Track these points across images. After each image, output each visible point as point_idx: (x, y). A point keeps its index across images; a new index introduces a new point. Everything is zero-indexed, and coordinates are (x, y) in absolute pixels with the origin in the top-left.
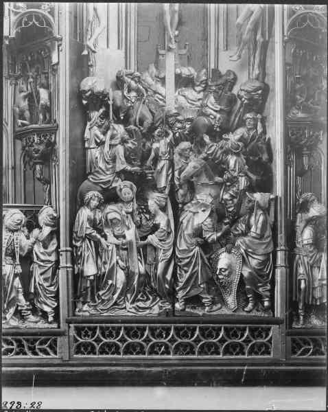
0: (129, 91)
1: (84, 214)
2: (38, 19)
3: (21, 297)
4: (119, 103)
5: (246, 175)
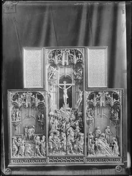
0: (58, 113)
1: (50, 137)
2: (42, 102)
3: (39, 152)
4: (56, 116)
5: (92, 139)
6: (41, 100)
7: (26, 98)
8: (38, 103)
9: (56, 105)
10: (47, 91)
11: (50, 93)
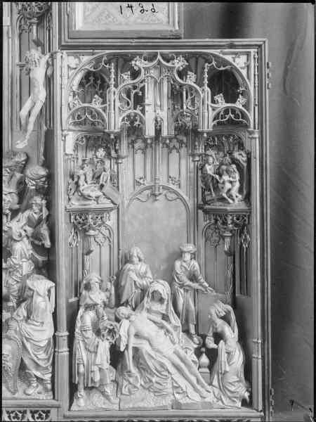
6: (232, 97)
7: (143, 89)
8: (212, 114)
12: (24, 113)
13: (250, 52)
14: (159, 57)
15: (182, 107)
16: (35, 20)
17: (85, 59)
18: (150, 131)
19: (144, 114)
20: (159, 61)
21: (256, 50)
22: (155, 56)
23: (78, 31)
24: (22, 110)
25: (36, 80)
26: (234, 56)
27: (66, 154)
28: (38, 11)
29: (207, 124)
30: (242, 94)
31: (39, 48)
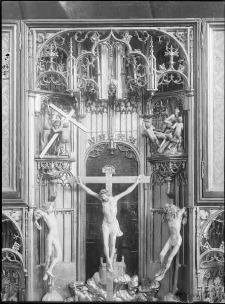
9: (74, 265)
10: (32, 204)
11: (44, 214)
12: (163, 253)
13: (187, 29)
14: (112, 33)
15: (133, 77)
16: (169, 178)
17: (213, 212)
18: (104, 95)
19: (97, 82)
20: (112, 37)
21: (192, 27)
22: (108, 33)
23: (210, 192)
24: (163, 251)
25: (175, 229)
26: (11, 211)
27: (198, 288)
28: (173, 172)
29: (153, 85)
30: (182, 64)
31: (172, 200)
